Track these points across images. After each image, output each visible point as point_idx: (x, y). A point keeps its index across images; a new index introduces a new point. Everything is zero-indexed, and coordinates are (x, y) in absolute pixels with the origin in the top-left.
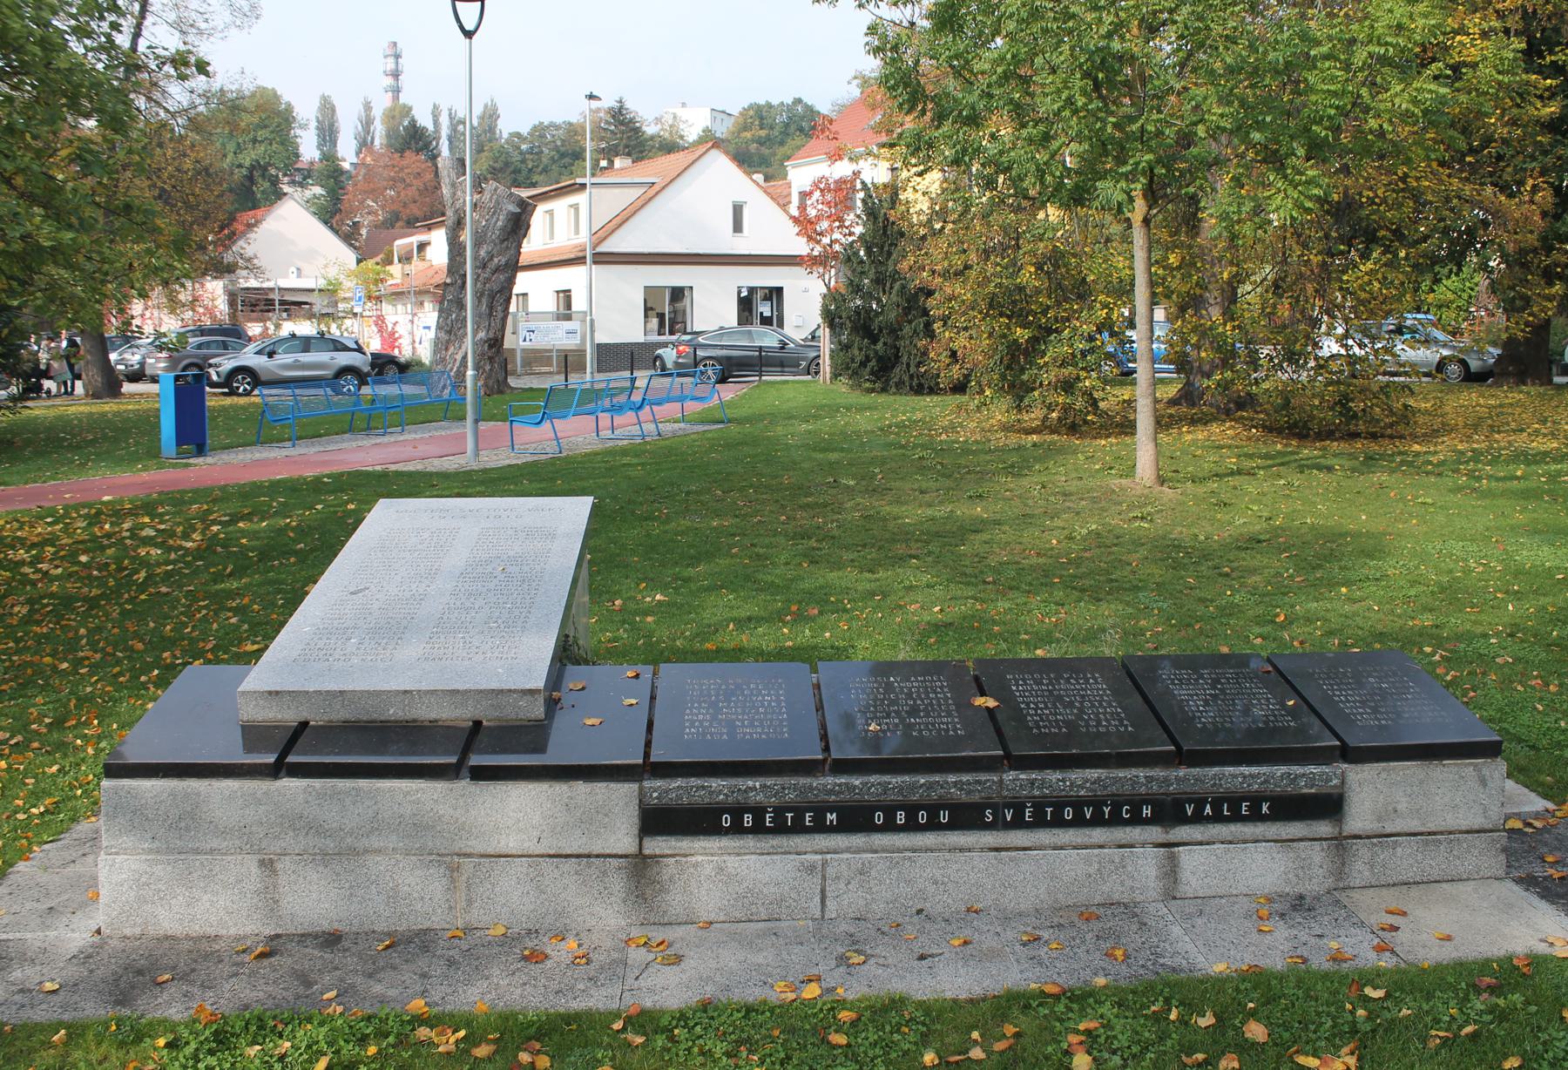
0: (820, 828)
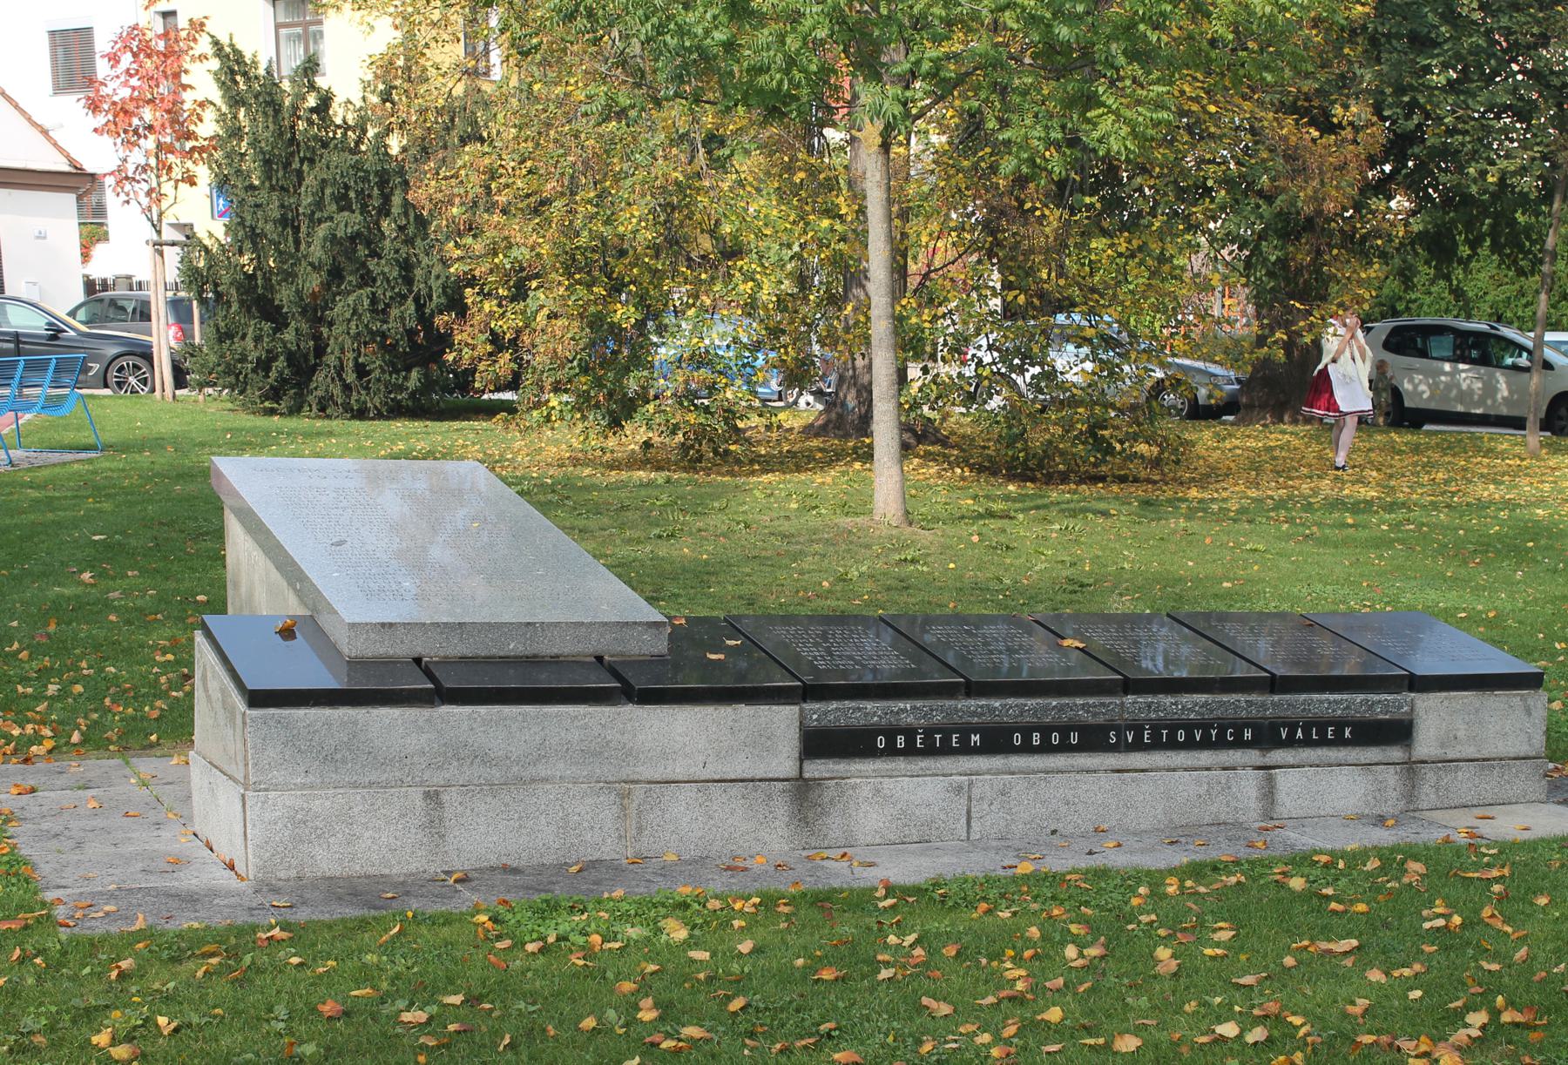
0: (966, 750)
